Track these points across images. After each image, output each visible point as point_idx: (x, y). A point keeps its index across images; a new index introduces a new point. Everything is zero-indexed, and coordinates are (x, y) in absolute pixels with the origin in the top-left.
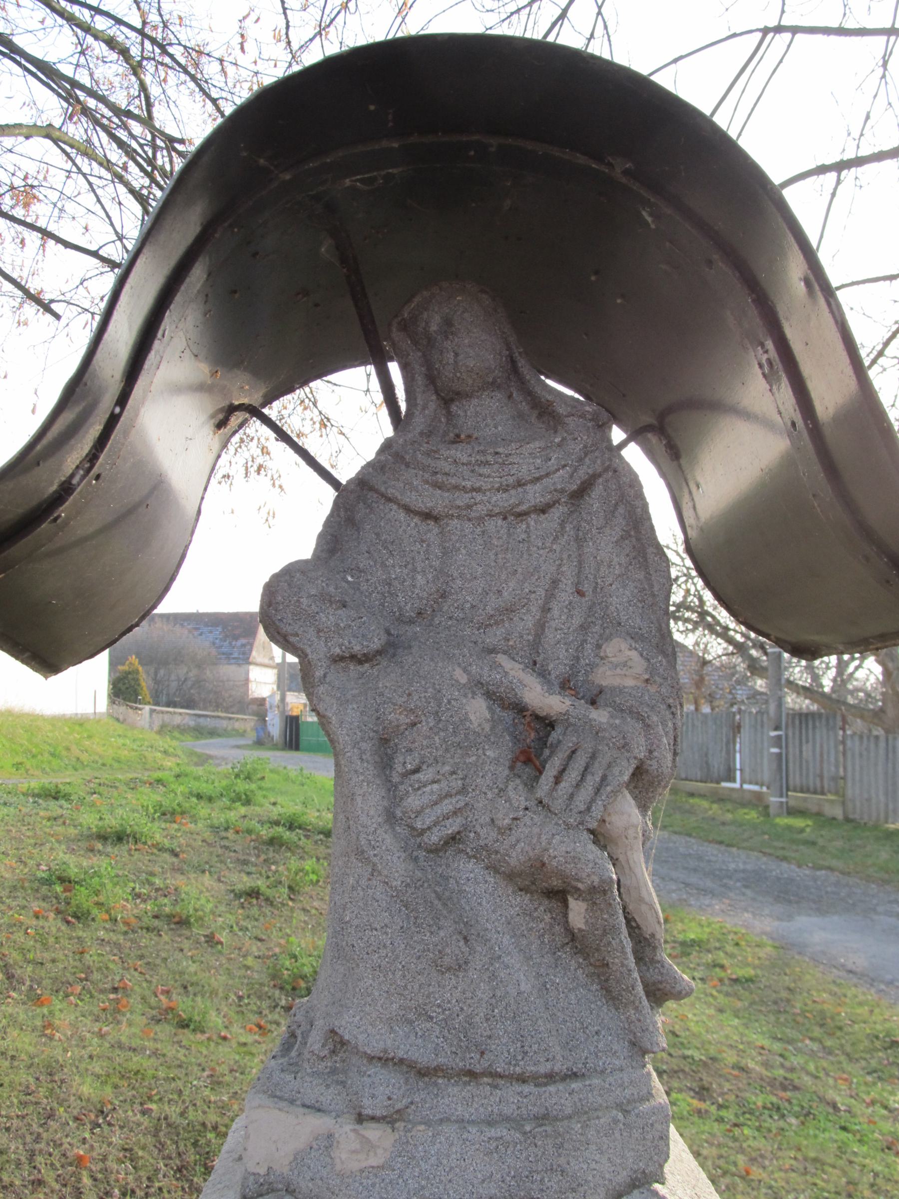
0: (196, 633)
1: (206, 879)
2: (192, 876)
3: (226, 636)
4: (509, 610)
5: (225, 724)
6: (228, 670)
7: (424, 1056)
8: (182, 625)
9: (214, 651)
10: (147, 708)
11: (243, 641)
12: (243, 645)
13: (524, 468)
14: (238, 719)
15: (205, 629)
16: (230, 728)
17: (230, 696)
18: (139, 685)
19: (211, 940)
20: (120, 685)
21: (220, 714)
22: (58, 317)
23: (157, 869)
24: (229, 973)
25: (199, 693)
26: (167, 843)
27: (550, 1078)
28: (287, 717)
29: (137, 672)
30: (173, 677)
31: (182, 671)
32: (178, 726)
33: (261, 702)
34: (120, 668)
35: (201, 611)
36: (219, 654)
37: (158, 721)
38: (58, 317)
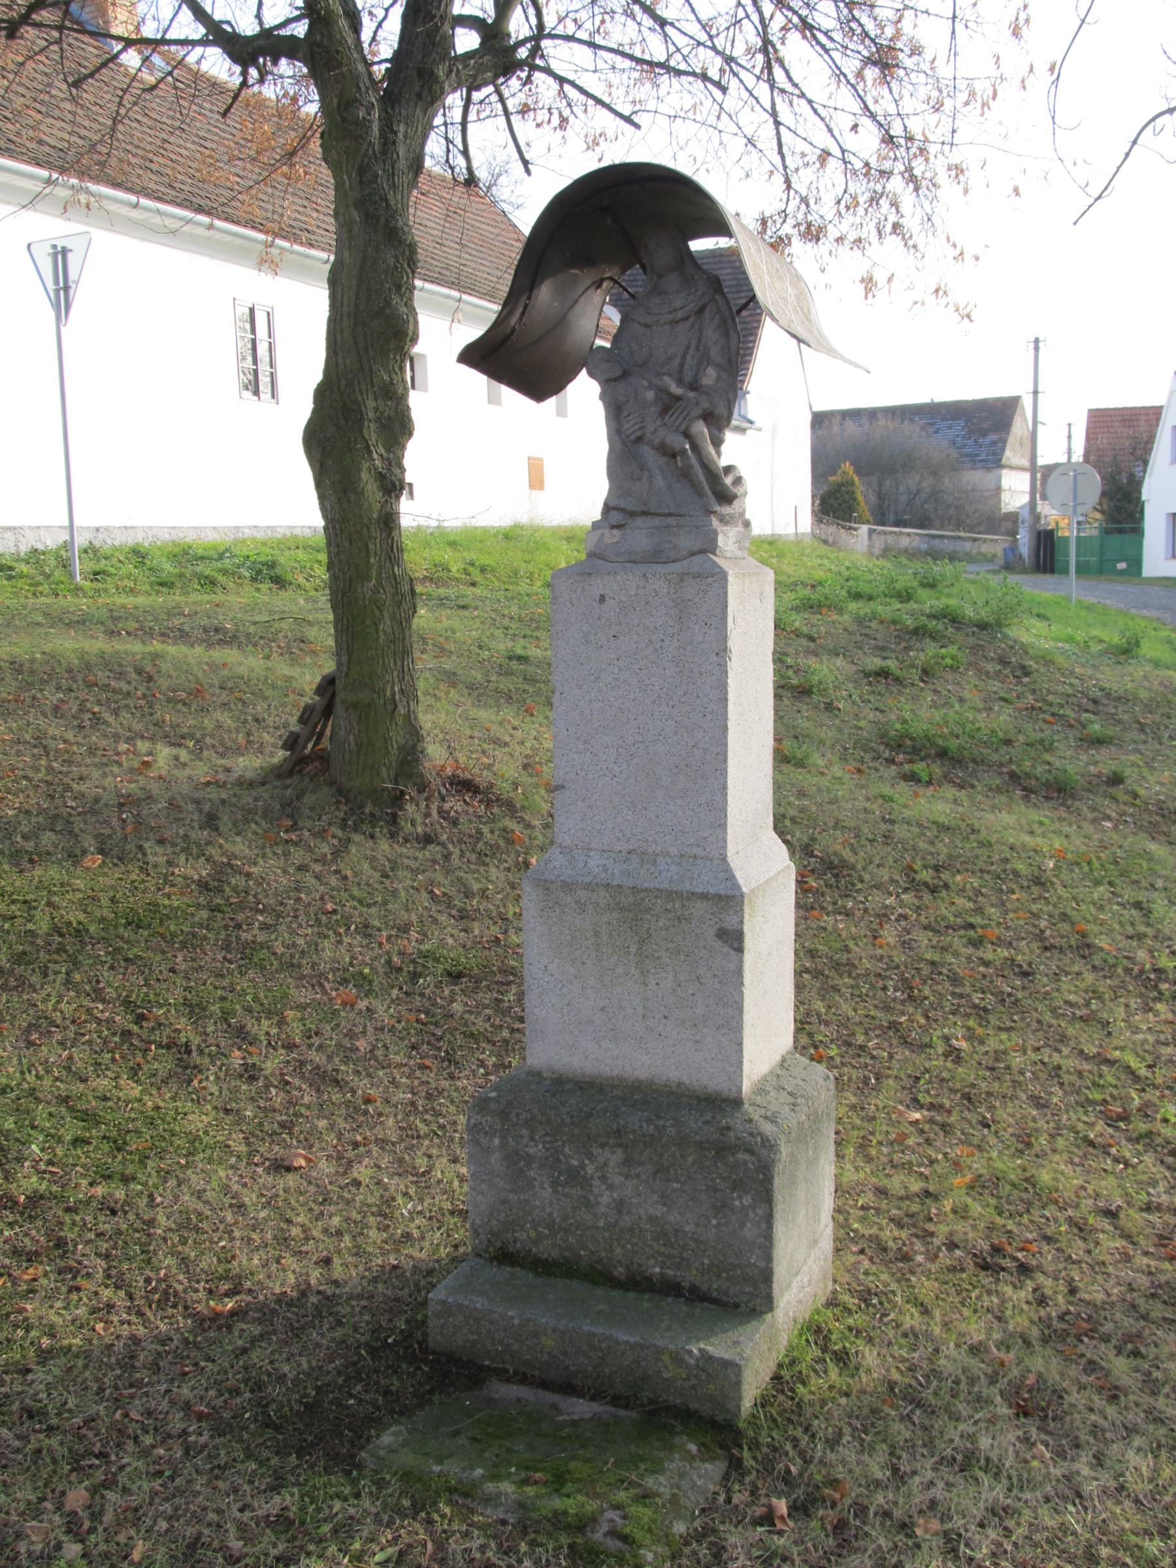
0: (931, 430)
1: (839, 662)
2: (825, 657)
3: (971, 432)
4: (670, 359)
5: (968, 546)
6: (974, 478)
7: (629, 507)
8: (911, 420)
9: (954, 454)
10: (864, 528)
11: (993, 437)
12: (994, 443)
13: (678, 303)
14: (985, 541)
15: (942, 424)
16: (974, 551)
17: (976, 511)
18: (855, 499)
19: (829, 707)
20: (832, 501)
21: (962, 534)
22: (638, 127)
23: (791, 650)
24: (840, 730)
25: (936, 509)
26: (805, 630)
27: (671, 515)
28: (1039, 534)
29: (852, 483)
30: (902, 489)
31: (912, 480)
32: (906, 550)
33: (1013, 517)
34: (832, 479)
35: (937, 400)
36: (961, 456)
37: (879, 542)
38: (638, 127)
